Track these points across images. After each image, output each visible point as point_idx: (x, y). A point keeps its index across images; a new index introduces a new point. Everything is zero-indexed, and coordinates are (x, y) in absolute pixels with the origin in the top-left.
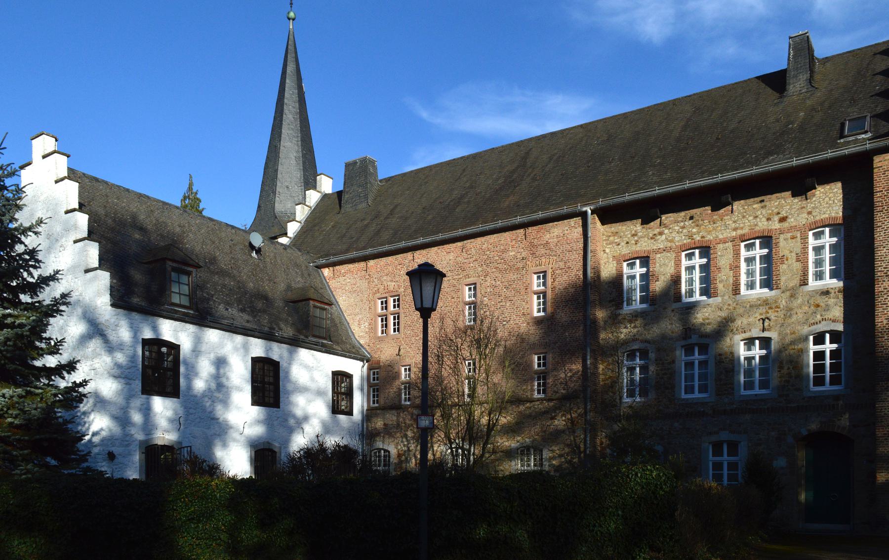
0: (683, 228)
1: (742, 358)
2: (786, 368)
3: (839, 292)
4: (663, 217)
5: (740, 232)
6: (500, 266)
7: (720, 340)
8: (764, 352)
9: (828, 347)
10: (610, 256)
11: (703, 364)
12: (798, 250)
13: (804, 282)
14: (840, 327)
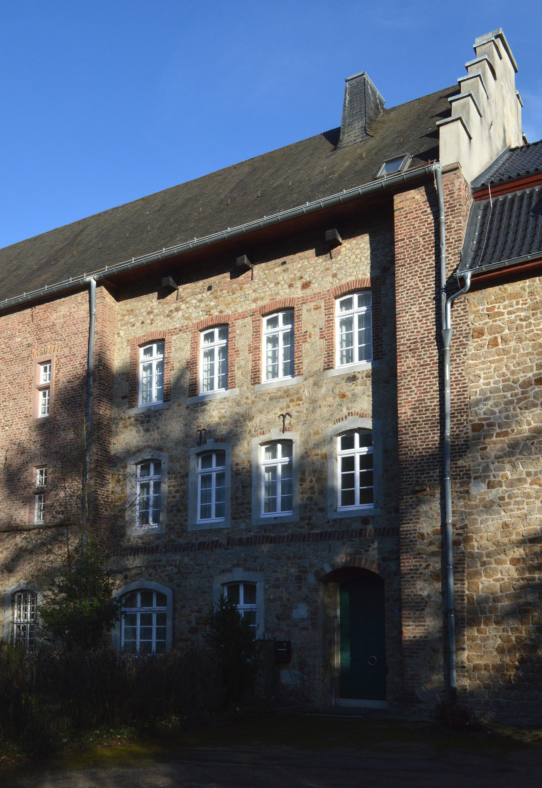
0: (200, 301)
1: (263, 468)
2: (308, 480)
3: (367, 376)
4: (181, 288)
5: (260, 303)
6: (6, 356)
7: (236, 445)
8: (287, 459)
9: (358, 451)
10: (124, 340)
11: (220, 477)
12: (322, 323)
13: (329, 366)
14: (368, 424)
